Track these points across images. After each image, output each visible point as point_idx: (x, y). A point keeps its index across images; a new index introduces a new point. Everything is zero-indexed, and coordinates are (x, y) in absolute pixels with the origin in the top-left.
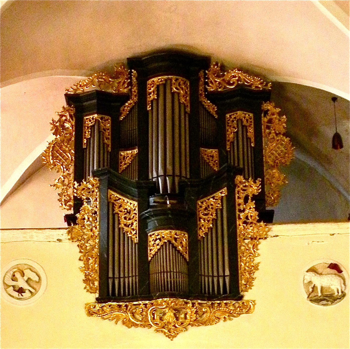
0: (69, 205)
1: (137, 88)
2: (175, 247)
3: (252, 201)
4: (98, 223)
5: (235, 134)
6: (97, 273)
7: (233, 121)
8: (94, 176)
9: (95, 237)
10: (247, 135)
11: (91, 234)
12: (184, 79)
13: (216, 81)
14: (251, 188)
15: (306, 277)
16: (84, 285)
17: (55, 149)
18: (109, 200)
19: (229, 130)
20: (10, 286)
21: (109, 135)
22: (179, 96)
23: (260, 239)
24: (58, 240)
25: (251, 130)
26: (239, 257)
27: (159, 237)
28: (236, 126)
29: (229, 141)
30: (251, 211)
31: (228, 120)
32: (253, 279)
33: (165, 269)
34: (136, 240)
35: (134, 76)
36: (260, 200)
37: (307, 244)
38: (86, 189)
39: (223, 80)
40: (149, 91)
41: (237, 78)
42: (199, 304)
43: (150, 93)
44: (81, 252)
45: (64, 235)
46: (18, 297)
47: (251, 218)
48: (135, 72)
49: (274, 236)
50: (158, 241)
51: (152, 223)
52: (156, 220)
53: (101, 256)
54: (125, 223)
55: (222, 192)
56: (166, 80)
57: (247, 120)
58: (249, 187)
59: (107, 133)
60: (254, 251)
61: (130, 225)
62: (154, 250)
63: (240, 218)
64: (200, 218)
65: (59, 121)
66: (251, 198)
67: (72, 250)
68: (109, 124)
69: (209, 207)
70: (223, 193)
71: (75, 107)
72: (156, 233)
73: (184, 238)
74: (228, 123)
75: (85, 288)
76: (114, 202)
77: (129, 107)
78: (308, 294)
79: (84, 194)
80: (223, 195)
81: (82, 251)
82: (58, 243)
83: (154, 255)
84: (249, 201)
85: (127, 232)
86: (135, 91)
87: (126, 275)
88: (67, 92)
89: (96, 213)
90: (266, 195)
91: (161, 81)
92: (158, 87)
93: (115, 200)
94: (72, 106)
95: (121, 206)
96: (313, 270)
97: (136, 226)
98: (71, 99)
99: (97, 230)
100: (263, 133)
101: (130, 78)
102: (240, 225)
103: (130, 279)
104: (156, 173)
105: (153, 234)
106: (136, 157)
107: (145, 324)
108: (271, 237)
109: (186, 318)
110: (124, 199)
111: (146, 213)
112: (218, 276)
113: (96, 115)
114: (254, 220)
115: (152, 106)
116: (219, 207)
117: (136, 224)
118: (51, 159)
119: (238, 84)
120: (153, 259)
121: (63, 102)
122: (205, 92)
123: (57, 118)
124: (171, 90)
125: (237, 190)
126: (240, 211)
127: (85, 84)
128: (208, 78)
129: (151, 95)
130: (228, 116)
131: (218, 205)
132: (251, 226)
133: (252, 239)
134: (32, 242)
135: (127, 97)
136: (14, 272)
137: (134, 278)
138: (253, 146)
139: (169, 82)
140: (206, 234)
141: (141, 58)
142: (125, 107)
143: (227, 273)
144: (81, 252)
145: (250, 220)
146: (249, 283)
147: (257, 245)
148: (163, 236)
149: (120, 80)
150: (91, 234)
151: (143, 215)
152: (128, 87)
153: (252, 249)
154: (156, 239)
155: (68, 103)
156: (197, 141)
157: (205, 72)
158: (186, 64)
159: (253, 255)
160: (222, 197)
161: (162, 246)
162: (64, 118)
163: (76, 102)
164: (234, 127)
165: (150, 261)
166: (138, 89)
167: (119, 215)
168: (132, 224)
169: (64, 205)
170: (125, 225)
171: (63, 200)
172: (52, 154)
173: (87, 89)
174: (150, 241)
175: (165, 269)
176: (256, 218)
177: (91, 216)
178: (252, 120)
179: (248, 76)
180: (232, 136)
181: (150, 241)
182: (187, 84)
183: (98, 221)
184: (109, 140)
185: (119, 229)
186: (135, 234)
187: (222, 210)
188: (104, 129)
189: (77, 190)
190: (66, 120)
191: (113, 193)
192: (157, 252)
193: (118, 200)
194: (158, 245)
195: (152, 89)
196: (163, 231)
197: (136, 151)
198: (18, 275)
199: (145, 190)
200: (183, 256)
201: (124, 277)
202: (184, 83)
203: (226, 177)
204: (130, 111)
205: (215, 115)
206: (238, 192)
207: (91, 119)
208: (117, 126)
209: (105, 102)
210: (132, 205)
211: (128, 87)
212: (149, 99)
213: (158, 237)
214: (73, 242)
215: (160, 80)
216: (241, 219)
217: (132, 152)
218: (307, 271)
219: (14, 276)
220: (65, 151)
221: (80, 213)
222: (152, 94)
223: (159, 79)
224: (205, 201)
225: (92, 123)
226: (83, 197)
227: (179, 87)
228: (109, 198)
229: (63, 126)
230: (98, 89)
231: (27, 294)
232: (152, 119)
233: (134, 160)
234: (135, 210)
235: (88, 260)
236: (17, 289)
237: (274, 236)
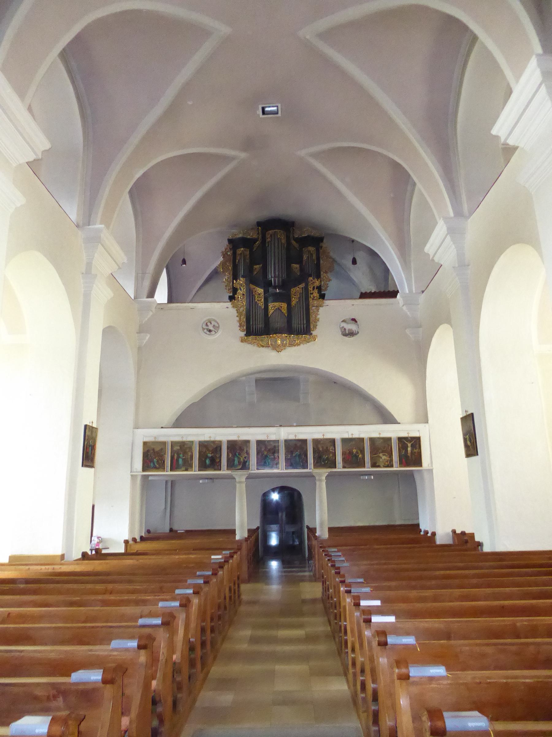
2: (281, 311)
17: (223, 264)
25: (314, 257)
30: (316, 294)
33: (278, 322)
34: (263, 307)
36: (319, 288)
51: (270, 299)
67: (233, 312)
70: (302, 285)
73: (284, 306)
92: (271, 236)
96: (343, 321)
98: (230, 241)
104: (271, 276)
113: (242, 249)
121: (226, 242)
126: (311, 294)
143: (305, 322)
146: (315, 327)
156: (289, 260)
158: (285, 225)
163: (234, 243)
173: (238, 236)
175: (278, 322)
197: (261, 265)
198: (209, 324)
199: (267, 285)
203: (303, 278)
209: (246, 242)
212: (267, 241)
213: (272, 306)
227: (281, 235)
231: (213, 333)
235: (241, 316)
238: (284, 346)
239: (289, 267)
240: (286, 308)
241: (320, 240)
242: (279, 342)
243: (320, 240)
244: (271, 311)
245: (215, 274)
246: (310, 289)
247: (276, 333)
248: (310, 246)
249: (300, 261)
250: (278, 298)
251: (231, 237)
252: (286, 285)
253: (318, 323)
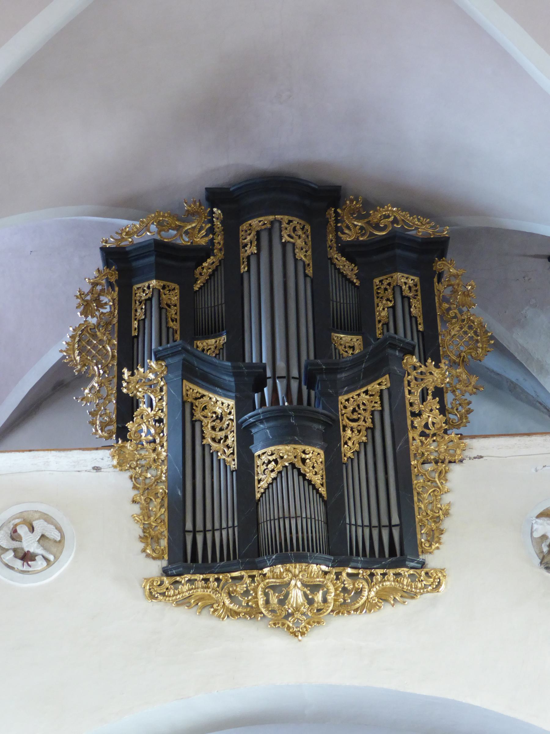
0: (109, 430)
1: (223, 237)
3: (434, 398)
4: (165, 439)
5: (391, 310)
6: (164, 524)
7: (386, 289)
8: (157, 359)
9: (160, 461)
10: (410, 312)
11: (154, 455)
12: (302, 222)
13: (356, 226)
14: (431, 376)
15: (535, 526)
16: (142, 545)
17: (84, 338)
18: (185, 399)
19: (380, 304)
20: (7, 550)
21: (176, 314)
22: (294, 250)
23: (450, 462)
24: (94, 468)
25: (416, 309)
26: (415, 494)
27: (274, 457)
28: (391, 297)
29: (380, 322)
30: (432, 416)
31: (378, 289)
32: (442, 532)
34: (234, 465)
35: (217, 219)
37: (533, 470)
38: (144, 380)
39: (368, 223)
40: (243, 241)
41: (391, 219)
42: (349, 575)
43: (246, 245)
44: (135, 487)
45: (106, 459)
46: (21, 568)
47: (434, 426)
48: (220, 212)
49: (475, 458)
50: (272, 465)
51: (260, 432)
52: (268, 428)
53: (171, 495)
54: (214, 437)
55: (382, 382)
56: (272, 223)
57: (410, 288)
58: (429, 374)
59: (173, 312)
60: (442, 483)
61: (221, 439)
62: (265, 480)
63: (413, 427)
64: (345, 427)
65: (91, 292)
66: (433, 392)
67: (118, 484)
68: (176, 296)
69: (359, 408)
70: (385, 382)
71: (117, 270)
72: (269, 450)
73: (315, 455)
74: (378, 293)
75: (144, 551)
76: (194, 401)
77: (209, 269)
78: (541, 557)
79: (140, 390)
80: (384, 387)
81: (138, 486)
82: (94, 474)
83: (265, 489)
84: (430, 397)
85: (217, 452)
86: (219, 243)
87: (217, 526)
88: (104, 244)
89: (160, 421)
90: (448, 410)
91: (264, 224)
92: (258, 233)
93: (196, 399)
94: (114, 267)
95: (205, 408)
97: (234, 441)
98: (113, 256)
99: (163, 450)
100: (437, 308)
101: (211, 221)
102: (414, 439)
103: (224, 533)
105: (263, 454)
106: (223, 349)
107: (252, 613)
108: (470, 458)
109: (325, 600)
110: (211, 395)
111: (250, 417)
112: (380, 527)
113: (154, 283)
114: (438, 429)
115: (249, 265)
116: (376, 408)
117: (233, 437)
118: (76, 354)
119: (394, 228)
120: (264, 495)
121: (98, 262)
122: (337, 243)
123: (87, 288)
124: (281, 239)
125: (407, 378)
126: (413, 414)
127: (135, 230)
128: (342, 221)
129: (246, 248)
130: (377, 281)
131: (376, 405)
132: (434, 441)
133: (437, 462)
134: (48, 472)
135: (205, 252)
136: (16, 525)
137: (230, 531)
138: (421, 330)
139: (277, 225)
140: (356, 453)
141: (229, 189)
142: (203, 268)
143: (395, 520)
144: (135, 487)
145: (433, 430)
146: (435, 536)
147: (446, 472)
148: (281, 455)
149: (194, 225)
150: (154, 455)
151: (246, 420)
152: (206, 235)
153: (437, 480)
154: (269, 462)
155: (107, 263)
156: (325, 323)
157: (335, 212)
158: (309, 197)
159: (438, 492)
160: (381, 391)
161: (280, 472)
162: (99, 288)
163: (120, 261)
164: (388, 300)
165: (259, 500)
166: (225, 239)
167: (203, 424)
168: (226, 437)
169: (100, 431)
170: (214, 440)
171: (98, 422)
172: (78, 346)
173: (137, 239)
174: (258, 466)
176: (441, 427)
177: (154, 426)
178: (419, 287)
179: (410, 217)
180: (384, 314)
181: (258, 466)
182: (307, 230)
183: (165, 434)
184: (176, 322)
185: (203, 446)
186: (231, 454)
187: (382, 412)
188: (167, 305)
189: (128, 383)
190: (102, 290)
191: (192, 386)
192: (272, 484)
193: (200, 398)
194: (273, 471)
195: (249, 238)
196: (280, 447)
197: (223, 339)
198: (23, 531)
199: (249, 383)
200: (317, 491)
201: (213, 530)
202: (303, 229)
203: (378, 361)
204: (211, 276)
205: (355, 281)
206: (409, 383)
207: (147, 287)
208: (188, 298)
209: (171, 260)
210: (224, 404)
211: (206, 235)
212: (243, 255)
213: (269, 458)
214: (121, 470)
215: (261, 222)
216: (416, 428)
217: (216, 342)
218: (538, 517)
219: (15, 531)
220: (101, 341)
221: (133, 421)
222: (249, 246)
223: (260, 221)
224: (353, 398)
225: (146, 294)
226: (138, 393)
227: (294, 233)
228: (184, 393)
229: (97, 300)
230: (158, 237)
231: (40, 564)
232: (250, 287)
233: (219, 354)
234: (230, 413)
235: (149, 501)
236: (21, 555)
237: (475, 458)
238: (316, 615)
239: (322, 344)
240: (320, 467)
241: (437, 247)
242: (297, 595)
243: (437, 247)
244: (264, 478)
245: (57, 386)
246: (413, 398)
247: (283, 560)
248: (396, 271)
249: (360, 323)
250: (291, 425)
251: (112, 243)
252: (324, 376)
253: (446, 524)
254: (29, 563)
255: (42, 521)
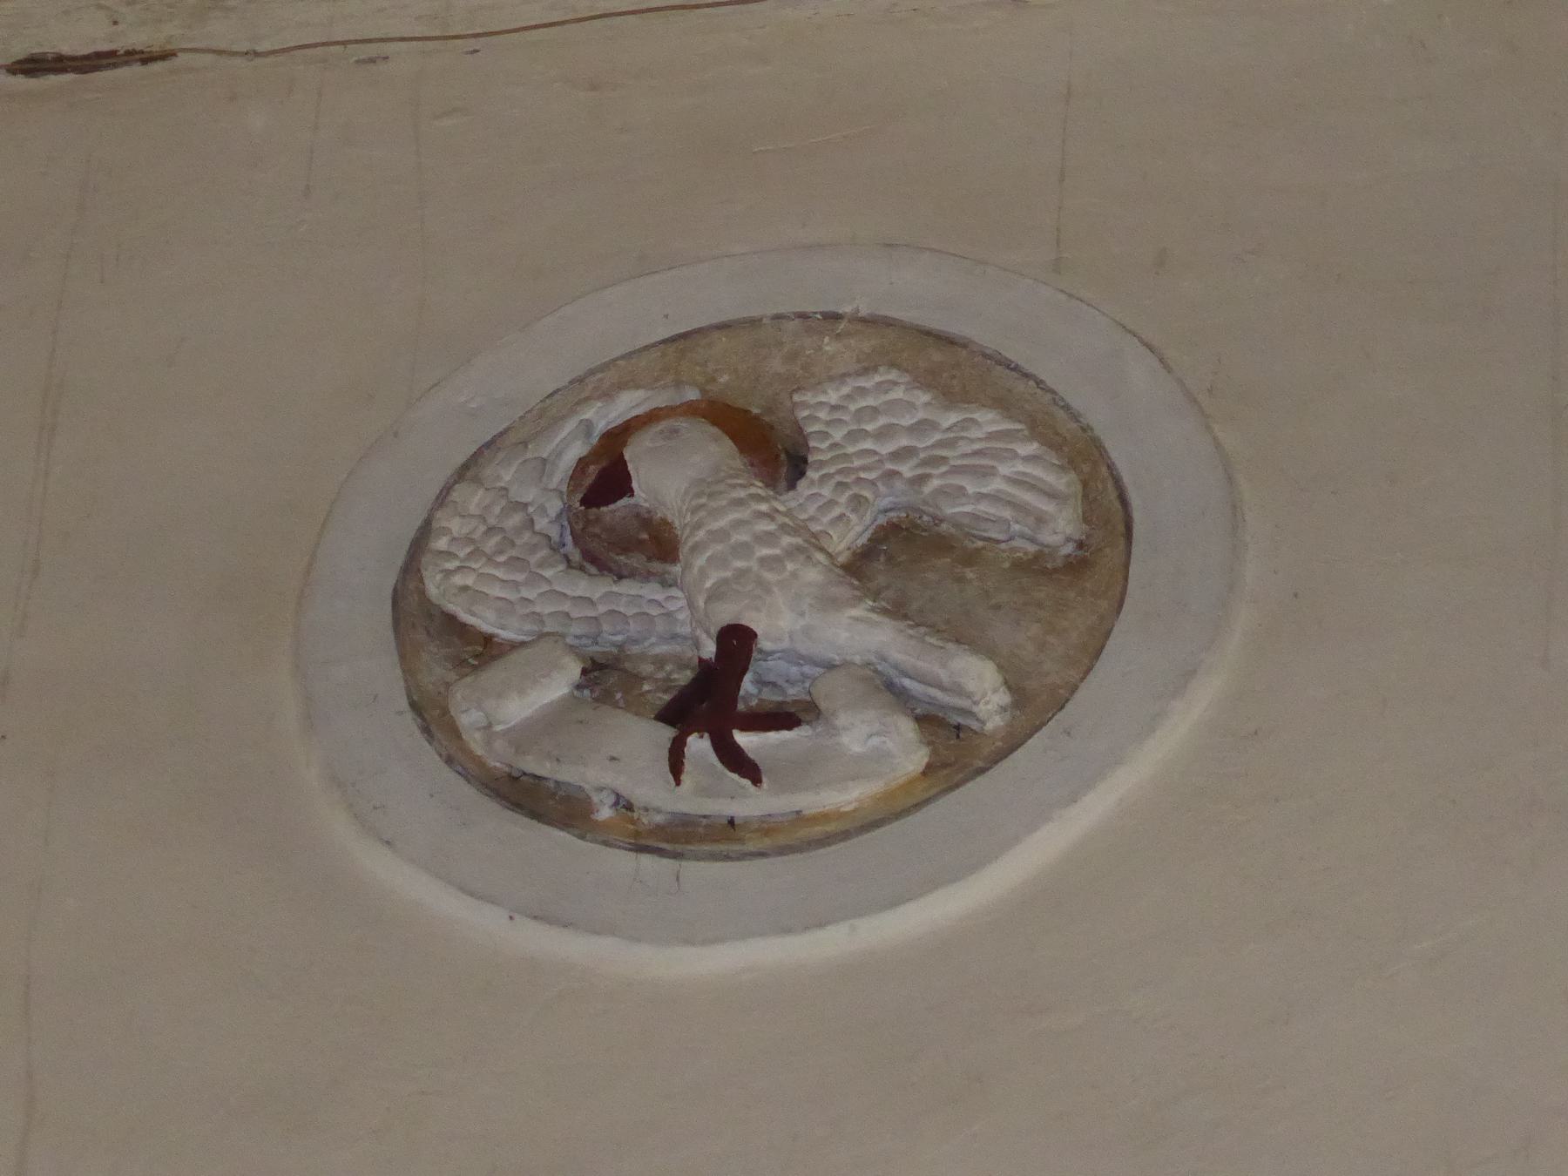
46: (659, 797)
136: (617, 437)
254: (742, 739)
255: (901, 401)
